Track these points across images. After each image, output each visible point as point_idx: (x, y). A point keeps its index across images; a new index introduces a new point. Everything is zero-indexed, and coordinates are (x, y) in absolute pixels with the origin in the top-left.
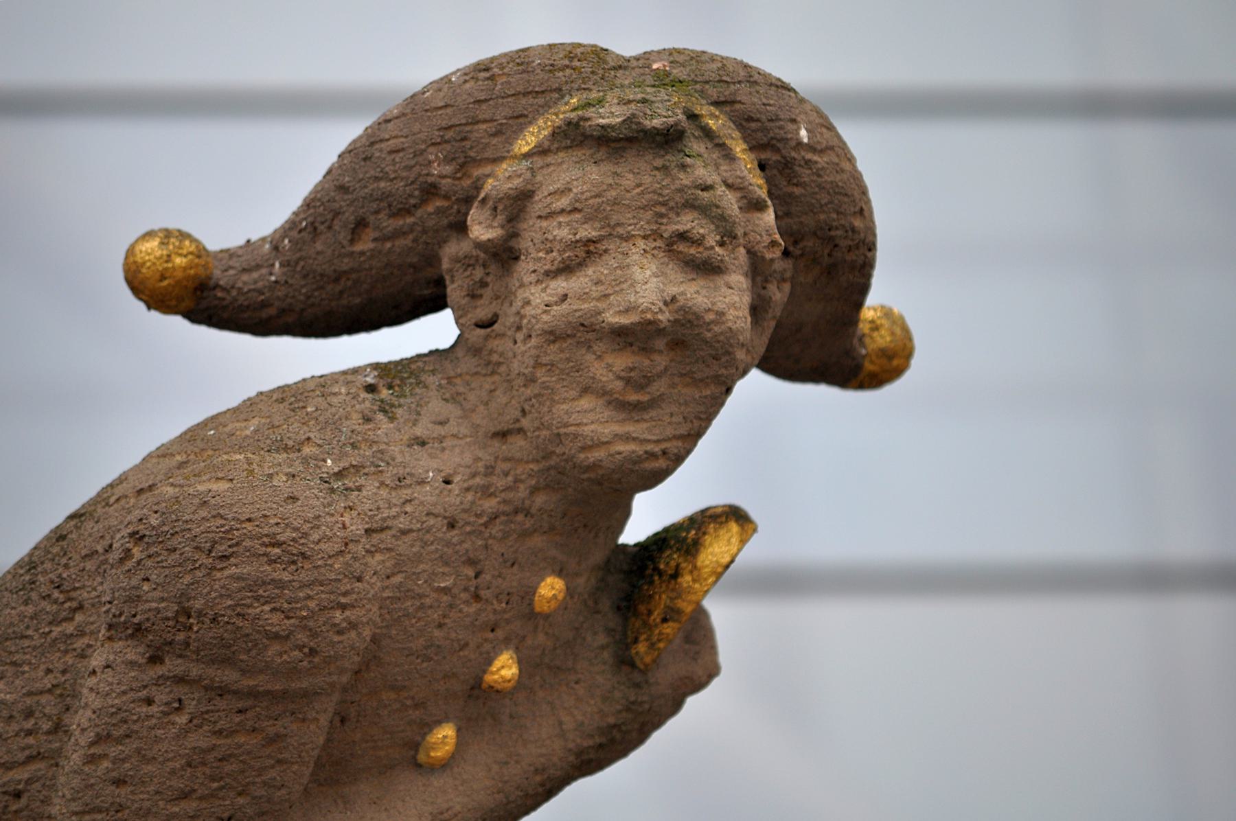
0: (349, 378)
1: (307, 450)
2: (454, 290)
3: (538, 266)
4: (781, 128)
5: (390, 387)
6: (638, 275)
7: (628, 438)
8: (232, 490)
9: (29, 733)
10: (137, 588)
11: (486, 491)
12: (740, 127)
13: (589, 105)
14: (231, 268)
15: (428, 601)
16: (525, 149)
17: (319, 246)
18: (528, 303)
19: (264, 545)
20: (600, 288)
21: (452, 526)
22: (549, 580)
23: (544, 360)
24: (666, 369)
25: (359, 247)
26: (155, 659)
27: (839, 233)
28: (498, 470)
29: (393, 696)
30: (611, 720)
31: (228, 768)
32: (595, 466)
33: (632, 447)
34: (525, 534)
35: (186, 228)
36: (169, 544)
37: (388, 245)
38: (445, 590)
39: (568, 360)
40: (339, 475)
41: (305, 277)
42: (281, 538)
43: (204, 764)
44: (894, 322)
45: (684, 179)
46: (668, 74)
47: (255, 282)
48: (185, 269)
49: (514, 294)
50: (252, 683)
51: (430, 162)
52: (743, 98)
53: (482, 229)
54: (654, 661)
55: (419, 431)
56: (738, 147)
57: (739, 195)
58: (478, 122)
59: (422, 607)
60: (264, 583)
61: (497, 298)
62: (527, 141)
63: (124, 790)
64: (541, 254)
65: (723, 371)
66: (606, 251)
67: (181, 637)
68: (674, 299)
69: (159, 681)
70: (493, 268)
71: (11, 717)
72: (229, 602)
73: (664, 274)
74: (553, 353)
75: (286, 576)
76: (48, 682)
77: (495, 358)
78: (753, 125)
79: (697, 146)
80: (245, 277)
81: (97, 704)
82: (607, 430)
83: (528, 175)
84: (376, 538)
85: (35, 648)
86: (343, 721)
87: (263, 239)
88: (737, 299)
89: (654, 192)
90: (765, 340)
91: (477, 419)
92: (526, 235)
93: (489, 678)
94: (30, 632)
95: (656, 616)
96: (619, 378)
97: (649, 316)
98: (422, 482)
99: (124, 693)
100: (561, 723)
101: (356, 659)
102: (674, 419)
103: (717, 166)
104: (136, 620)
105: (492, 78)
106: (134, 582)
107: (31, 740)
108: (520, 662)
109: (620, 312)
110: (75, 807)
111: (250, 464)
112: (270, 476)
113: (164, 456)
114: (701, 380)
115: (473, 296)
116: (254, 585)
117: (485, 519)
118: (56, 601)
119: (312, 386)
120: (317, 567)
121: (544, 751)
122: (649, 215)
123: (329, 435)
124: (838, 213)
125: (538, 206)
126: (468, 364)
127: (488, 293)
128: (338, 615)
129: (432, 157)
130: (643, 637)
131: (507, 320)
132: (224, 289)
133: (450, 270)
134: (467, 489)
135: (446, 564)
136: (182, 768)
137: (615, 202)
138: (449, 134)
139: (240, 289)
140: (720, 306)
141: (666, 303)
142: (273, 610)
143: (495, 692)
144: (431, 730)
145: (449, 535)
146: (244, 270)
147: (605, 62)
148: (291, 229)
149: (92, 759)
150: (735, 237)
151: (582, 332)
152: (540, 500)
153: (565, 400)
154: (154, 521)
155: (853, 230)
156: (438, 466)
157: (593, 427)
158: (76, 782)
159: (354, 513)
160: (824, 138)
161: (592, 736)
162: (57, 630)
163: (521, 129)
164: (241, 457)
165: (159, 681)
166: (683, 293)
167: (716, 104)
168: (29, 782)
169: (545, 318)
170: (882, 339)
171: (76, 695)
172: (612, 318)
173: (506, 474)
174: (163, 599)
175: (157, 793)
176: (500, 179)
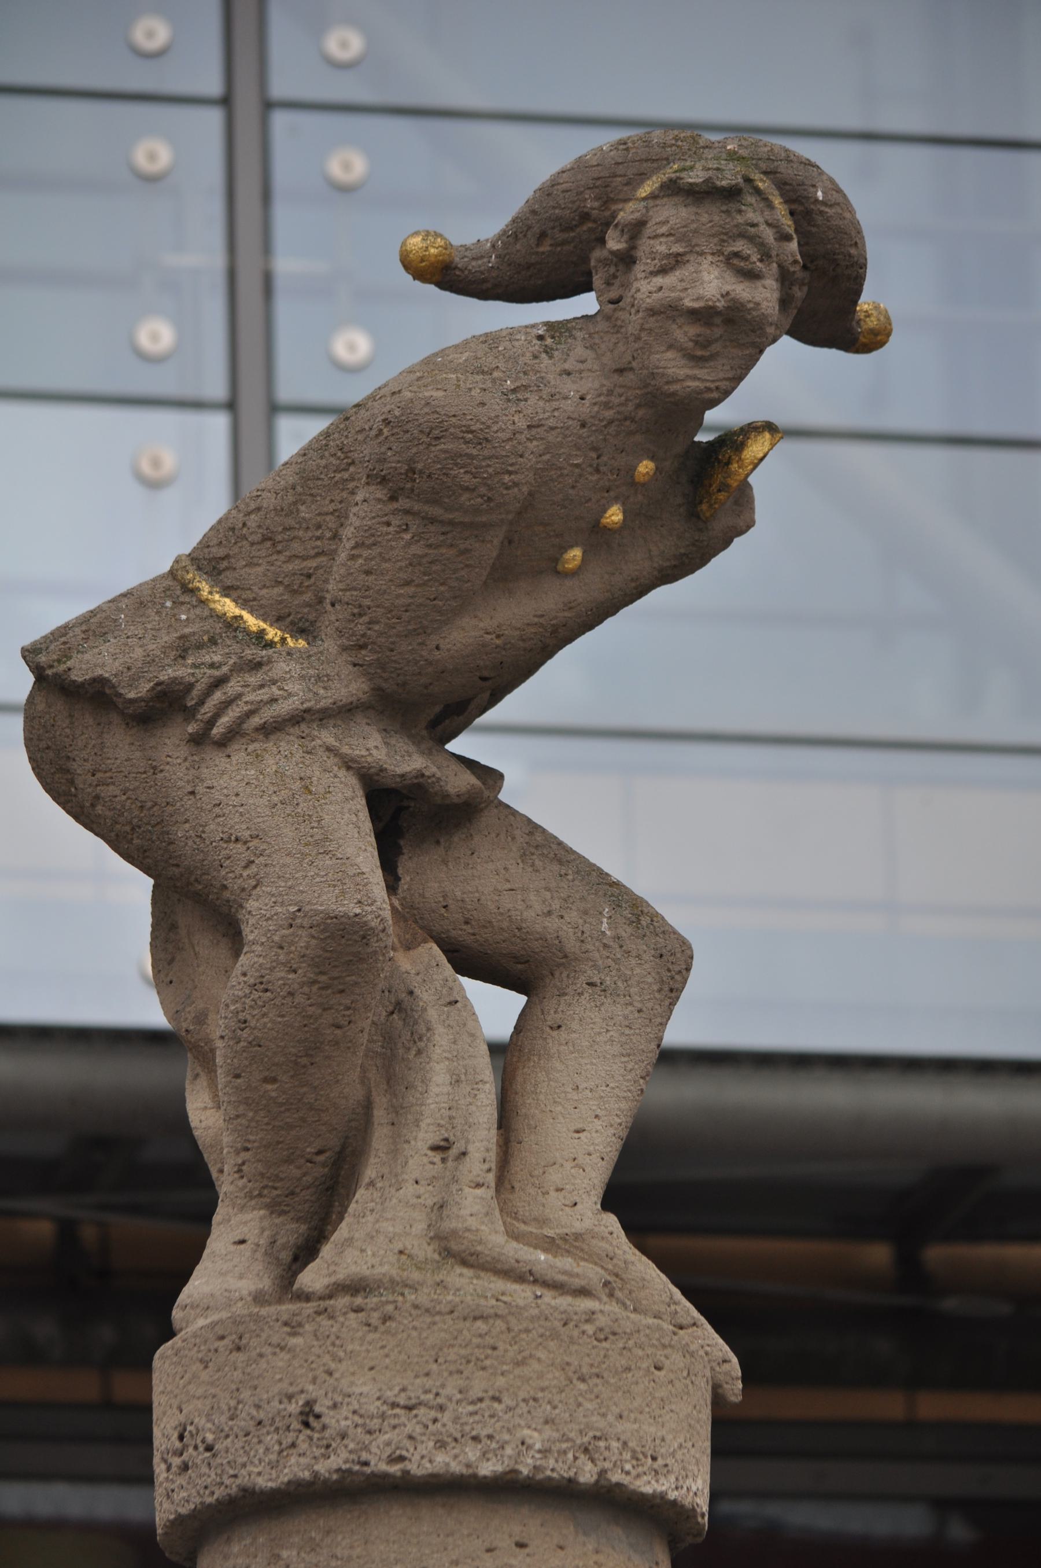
0: (528, 330)
1: (496, 374)
2: (597, 280)
3: (646, 268)
4: (805, 190)
5: (553, 337)
6: (706, 276)
7: (695, 378)
8: (445, 397)
9: (318, 538)
10: (384, 453)
11: (607, 406)
12: (779, 188)
13: (684, 169)
14: (465, 257)
15: (566, 472)
16: (644, 195)
17: (518, 247)
18: (638, 290)
19: (462, 431)
20: (683, 284)
21: (583, 425)
22: (645, 462)
23: (647, 326)
24: (721, 336)
25: (541, 249)
26: (393, 498)
27: (840, 257)
28: (615, 393)
29: (541, 528)
30: (682, 551)
31: (434, 568)
32: (674, 394)
33: (696, 384)
34: (631, 433)
35: (439, 231)
36: (405, 428)
37: (559, 249)
38: (577, 466)
39: (661, 327)
40: (514, 391)
41: (510, 265)
42: (473, 428)
43: (420, 564)
44: (880, 313)
45: (740, 219)
46: (735, 153)
47: (480, 266)
48: (436, 256)
49: (632, 284)
50: (451, 516)
51: (586, 199)
52: (783, 171)
53: (614, 243)
54: (711, 516)
55: (567, 366)
56: (777, 201)
57: (774, 230)
58: (616, 176)
59: (562, 475)
60: (461, 455)
61: (623, 286)
62: (645, 190)
63: (371, 578)
64: (649, 261)
65: (757, 339)
66: (688, 261)
67: (409, 485)
68: (728, 293)
69: (395, 512)
70: (621, 267)
71: (308, 528)
72: (439, 466)
73: (723, 278)
74: (652, 323)
75: (475, 452)
76: (331, 509)
77: (619, 323)
78: (788, 187)
79: (751, 199)
80: (474, 263)
81: (357, 523)
82: (682, 373)
83: (644, 211)
84: (534, 431)
85: (324, 486)
86: (510, 542)
87: (487, 240)
88: (769, 295)
89: (720, 226)
90: (790, 321)
91: (605, 360)
92: (641, 248)
93: (604, 521)
94: (322, 476)
95: (714, 488)
96: (691, 340)
97: (710, 303)
98: (566, 398)
99: (374, 518)
100: (650, 551)
101: (518, 505)
102: (725, 368)
103: (762, 212)
104: (383, 473)
105: (627, 149)
106: (383, 449)
107: (319, 543)
108: (624, 513)
109: (693, 300)
110: (341, 586)
111: (459, 381)
112: (470, 389)
113: (410, 372)
114: (743, 345)
115: (608, 284)
116: (455, 456)
117: (605, 423)
118: (339, 458)
119: (504, 333)
120: (495, 448)
121: (638, 567)
122: (716, 240)
123: (510, 366)
124: (840, 245)
125: (648, 231)
126: (602, 325)
127: (617, 282)
128: (506, 478)
129: (587, 196)
130: (705, 500)
131: (628, 300)
132: (460, 270)
133: (595, 267)
134: (595, 404)
135: (579, 449)
136: (406, 567)
137: (696, 231)
138: (599, 183)
139: (470, 270)
140: (757, 299)
141: (722, 296)
142: (466, 472)
143: (608, 530)
144: (566, 551)
145: (581, 432)
146: (473, 259)
147: (698, 143)
148: (503, 235)
149: (353, 558)
150: (770, 257)
151: (670, 311)
152: (641, 413)
153: (657, 353)
154: (397, 413)
155: (850, 255)
156: (576, 389)
157: (673, 370)
158: (342, 571)
159: (521, 415)
160: (835, 197)
161: (668, 560)
162: (338, 476)
163: (642, 182)
164: (454, 376)
165: (395, 512)
166: (734, 290)
167: (765, 173)
168: (316, 568)
169: (648, 300)
170: (872, 323)
171: (347, 517)
172: (688, 303)
173: (620, 396)
174: (399, 462)
175: (391, 581)
176: (628, 213)
